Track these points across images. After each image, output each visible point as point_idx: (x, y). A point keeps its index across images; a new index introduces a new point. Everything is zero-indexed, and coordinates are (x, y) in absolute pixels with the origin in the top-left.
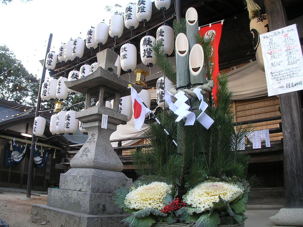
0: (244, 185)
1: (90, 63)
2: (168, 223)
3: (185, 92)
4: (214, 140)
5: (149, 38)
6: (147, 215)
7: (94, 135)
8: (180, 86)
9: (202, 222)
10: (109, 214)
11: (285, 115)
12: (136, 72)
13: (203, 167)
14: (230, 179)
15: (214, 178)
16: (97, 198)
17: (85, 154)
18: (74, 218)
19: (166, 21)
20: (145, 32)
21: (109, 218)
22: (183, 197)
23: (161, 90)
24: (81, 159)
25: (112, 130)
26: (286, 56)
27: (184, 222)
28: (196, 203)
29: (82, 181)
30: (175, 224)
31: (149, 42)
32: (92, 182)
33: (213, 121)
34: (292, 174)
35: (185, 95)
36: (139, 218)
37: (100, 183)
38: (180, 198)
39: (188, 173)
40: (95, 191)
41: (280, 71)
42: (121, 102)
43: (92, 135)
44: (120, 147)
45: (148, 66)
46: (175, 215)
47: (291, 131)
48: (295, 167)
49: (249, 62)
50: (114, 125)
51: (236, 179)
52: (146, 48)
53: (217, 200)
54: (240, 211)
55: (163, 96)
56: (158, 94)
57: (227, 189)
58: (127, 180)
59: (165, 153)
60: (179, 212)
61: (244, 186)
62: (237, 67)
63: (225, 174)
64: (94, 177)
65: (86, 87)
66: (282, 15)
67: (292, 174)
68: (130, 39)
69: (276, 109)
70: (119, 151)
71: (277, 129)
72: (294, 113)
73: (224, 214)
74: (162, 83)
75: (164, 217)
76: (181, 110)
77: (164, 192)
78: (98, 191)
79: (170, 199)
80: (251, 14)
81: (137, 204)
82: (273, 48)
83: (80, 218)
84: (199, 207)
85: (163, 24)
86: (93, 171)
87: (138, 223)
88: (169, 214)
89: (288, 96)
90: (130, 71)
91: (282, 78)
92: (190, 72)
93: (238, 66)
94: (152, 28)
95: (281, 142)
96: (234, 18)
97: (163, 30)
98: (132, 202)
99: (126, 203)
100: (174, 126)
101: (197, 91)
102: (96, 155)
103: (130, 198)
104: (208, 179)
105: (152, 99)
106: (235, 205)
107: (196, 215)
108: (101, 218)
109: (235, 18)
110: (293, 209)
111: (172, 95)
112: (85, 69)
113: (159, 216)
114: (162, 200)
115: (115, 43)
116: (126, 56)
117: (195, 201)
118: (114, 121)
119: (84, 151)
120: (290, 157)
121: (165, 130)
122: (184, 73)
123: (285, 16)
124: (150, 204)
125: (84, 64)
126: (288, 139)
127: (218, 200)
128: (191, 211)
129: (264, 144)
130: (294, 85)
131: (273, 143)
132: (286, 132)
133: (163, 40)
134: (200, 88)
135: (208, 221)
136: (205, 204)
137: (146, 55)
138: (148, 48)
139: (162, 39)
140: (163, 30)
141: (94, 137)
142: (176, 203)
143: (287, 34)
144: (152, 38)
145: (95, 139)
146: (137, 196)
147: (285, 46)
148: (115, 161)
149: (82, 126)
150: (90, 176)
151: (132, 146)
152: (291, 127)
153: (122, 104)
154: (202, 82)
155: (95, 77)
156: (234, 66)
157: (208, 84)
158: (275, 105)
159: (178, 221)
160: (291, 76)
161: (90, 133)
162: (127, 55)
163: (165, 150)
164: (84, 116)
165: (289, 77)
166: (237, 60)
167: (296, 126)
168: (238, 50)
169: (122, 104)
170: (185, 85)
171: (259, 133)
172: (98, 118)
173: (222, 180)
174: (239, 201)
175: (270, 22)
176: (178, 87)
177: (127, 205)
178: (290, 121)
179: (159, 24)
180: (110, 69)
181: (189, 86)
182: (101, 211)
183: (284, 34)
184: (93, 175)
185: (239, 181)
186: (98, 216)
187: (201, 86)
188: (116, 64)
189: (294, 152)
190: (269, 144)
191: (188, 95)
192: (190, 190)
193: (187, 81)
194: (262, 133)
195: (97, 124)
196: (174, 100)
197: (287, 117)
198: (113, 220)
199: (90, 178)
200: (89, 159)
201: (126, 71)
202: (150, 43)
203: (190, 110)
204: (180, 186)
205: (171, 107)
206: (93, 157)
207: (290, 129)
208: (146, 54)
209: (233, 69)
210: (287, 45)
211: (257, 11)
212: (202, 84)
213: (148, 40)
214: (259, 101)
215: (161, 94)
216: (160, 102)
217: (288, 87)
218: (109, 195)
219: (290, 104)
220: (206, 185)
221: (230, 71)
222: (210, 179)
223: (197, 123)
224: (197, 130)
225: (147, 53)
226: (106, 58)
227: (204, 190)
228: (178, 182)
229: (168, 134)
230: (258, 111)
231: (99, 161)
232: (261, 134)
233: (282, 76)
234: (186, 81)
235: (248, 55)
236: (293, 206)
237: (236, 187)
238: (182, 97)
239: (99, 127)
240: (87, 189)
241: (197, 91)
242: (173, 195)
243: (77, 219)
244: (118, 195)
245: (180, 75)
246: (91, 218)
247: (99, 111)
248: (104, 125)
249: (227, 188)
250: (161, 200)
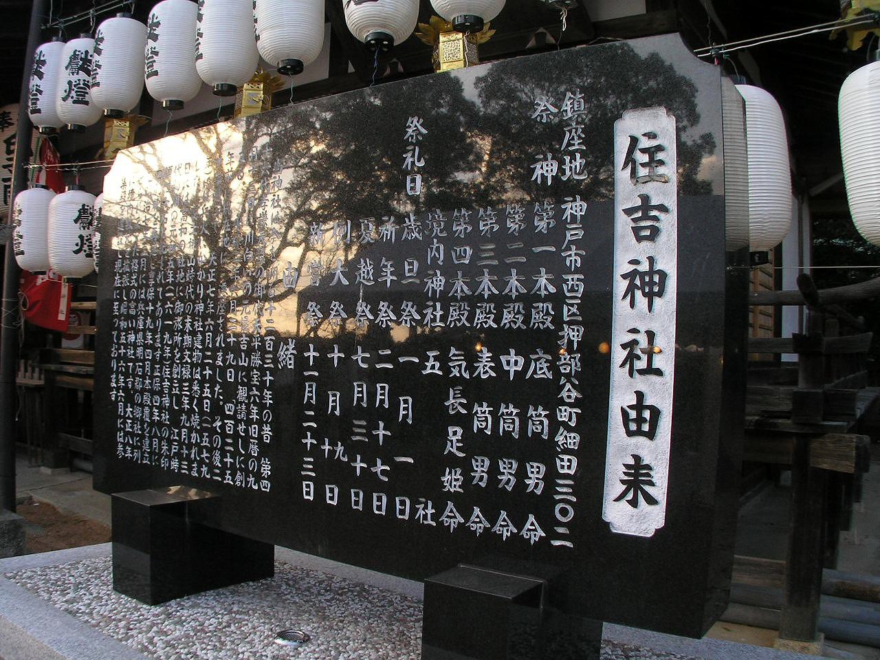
133: (5, 167)
153: (656, 529)
208: (73, 94)
225: (76, 92)
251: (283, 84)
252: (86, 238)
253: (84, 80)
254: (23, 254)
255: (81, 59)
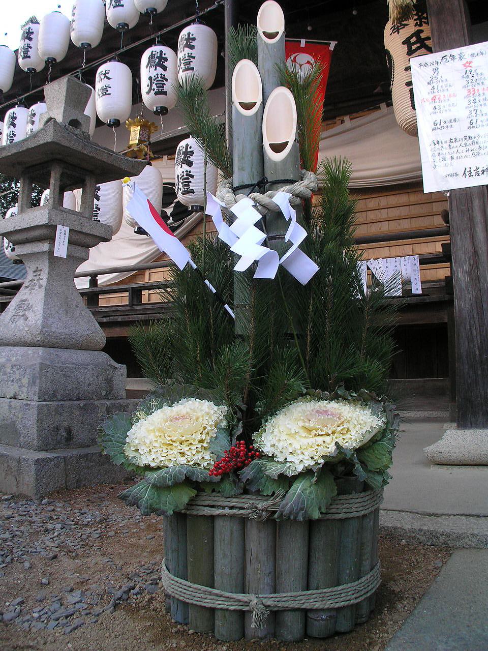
0: (384, 411)
1: (28, 103)
2: (225, 496)
3: (254, 200)
4: (317, 307)
5: (161, 52)
6: (177, 481)
7: (41, 270)
8: (241, 184)
9: (300, 496)
10: (82, 446)
11: (458, 234)
12: (130, 124)
13: (296, 373)
14: (354, 394)
15: (319, 393)
16: (54, 413)
17: (20, 314)
18: (7, 460)
19: (201, 14)
20: (152, 37)
21: (81, 457)
22: (254, 436)
23: (185, 167)
24: (13, 326)
25: (79, 258)
26: (466, 108)
27: (258, 492)
28: (284, 451)
29: (17, 375)
30: (238, 496)
31: (160, 62)
32: (41, 379)
33: (316, 268)
34: (470, 359)
35: (255, 206)
36: (160, 487)
37: (57, 379)
38: (247, 438)
39: (261, 383)
40: (47, 397)
41: (451, 139)
42: (98, 192)
43: (34, 272)
44: (95, 289)
45: (157, 113)
46: (239, 480)
47: (471, 270)
48: (477, 346)
49: (379, 108)
50: (83, 248)
51: (366, 396)
52: (153, 73)
53: (330, 446)
54: (377, 467)
55: (191, 182)
56: (180, 176)
57: (350, 419)
58: (115, 368)
59: (208, 332)
60: (248, 473)
61: (385, 414)
62: (352, 116)
63: (342, 383)
64: (43, 366)
65: (19, 164)
66: (461, 18)
67: (470, 359)
68: (118, 52)
69: (434, 210)
70: (92, 297)
71: (437, 255)
72: (478, 232)
73: (343, 471)
74: (188, 153)
75: (215, 482)
76: (247, 245)
77: (211, 426)
78: (53, 397)
79: (224, 441)
80: (393, 13)
81: (153, 456)
82: (439, 88)
83: (19, 461)
84: (291, 462)
85: (193, 21)
86: (40, 353)
87: (159, 496)
88: (225, 476)
89: (466, 193)
90: (116, 123)
91: (455, 156)
92: (266, 152)
93: (354, 115)
94: (169, 29)
95: (444, 283)
96: (354, 15)
97: (192, 35)
98: (143, 449)
99: (130, 453)
100: (230, 274)
101: (281, 198)
102: (45, 318)
103: (137, 441)
104: (306, 394)
105: (165, 181)
106: (366, 454)
107: (286, 481)
108: (64, 458)
109: (354, 13)
110: (472, 431)
111: (224, 206)
112: (15, 118)
113: (204, 482)
114: (207, 443)
115: (84, 61)
116: (107, 91)
117: (281, 448)
118: (82, 239)
119: (19, 307)
120: (468, 323)
121: (207, 282)
122: (252, 154)
123: (467, 22)
124: (182, 454)
125: (12, 106)
126: (463, 286)
127: (332, 449)
128: (273, 470)
129: (407, 287)
130: (480, 173)
131: (427, 285)
132: (459, 272)
133: (194, 58)
134: (289, 192)
135: (311, 493)
136: (303, 456)
137: (154, 90)
138: (157, 75)
139: (191, 54)
140: (192, 35)
141: (40, 275)
142: (240, 452)
143: (471, 62)
144: (167, 51)
145: (42, 279)
146: (152, 437)
147: (464, 87)
148: (87, 326)
149: (10, 247)
150: (35, 364)
151: (120, 287)
152: (472, 262)
153: (99, 197)
154: (291, 177)
155: (41, 142)
156: (346, 114)
157: (306, 182)
158: (432, 202)
159: (246, 492)
160: (475, 152)
161: (30, 267)
162: (110, 87)
163: (208, 327)
164: (16, 228)
165: (470, 153)
166: (351, 103)
167: (483, 258)
168: (356, 87)
169: (99, 197)
170: (253, 183)
171: (397, 264)
172: (47, 233)
173: (335, 398)
174: (376, 446)
175: (436, 34)
176: (236, 185)
177: (133, 458)
178: (470, 248)
179: (185, 21)
180: (75, 123)
181: (262, 185)
182: (64, 441)
183: (464, 61)
184: (42, 363)
185: (372, 399)
186: (57, 455)
187: (289, 187)
188: (88, 111)
189: (475, 314)
190: (419, 286)
191: (260, 208)
192: (266, 421)
193: (258, 172)
194: (403, 263)
195: (45, 247)
196: (230, 218)
197: (463, 238)
198: (91, 459)
199: (34, 369)
200: (30, 326)
201: (109, 122)
202: (163, 62)
203: (265, 244)
204: (245, 409)
205: (224, 233)
206: (39, 322)
207: (470, 264)
208: (154, 86)
209: (343, 122)
210: (470, 84)
211: (408, 7)
212: (292, 182)
213: (158, 55)
214: (397, 192)
215: (185, 177)
216: (183, 193)
217: (468, 176)
218: (79, 404)
219: (470, 212)
220: (302, 410)
221: (336, 125)
222: (310, 395)
223: (283, 271)
224: (280, 288)
225: (156, 84)
226: (66, 97)
227: (301, 424)
228: (239, 402)
229: (214, 291)
230: (394, 213)
231: (53, 330)
232: (403, 265)
233: (455, 150)
234: (256, 173)
235: (378, 94)
236: (471, 424)
237: (368, 412)
238: (247, 211)
239: (51, 252)
240: (30, 394)
241: (281, 198)
242: (230, 431)
243: (14, 464)
244: (109, 435)
245: (241, 158)
246: (44, 460)
247: (50, 219)
248: (61, 249)
249: (350, 417)
250: (205, 445)
251: (242, 26)
252: (153, 78)
253: (187, 171)
254: (193, 193)
255: (157, 57)
